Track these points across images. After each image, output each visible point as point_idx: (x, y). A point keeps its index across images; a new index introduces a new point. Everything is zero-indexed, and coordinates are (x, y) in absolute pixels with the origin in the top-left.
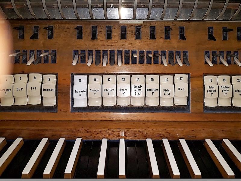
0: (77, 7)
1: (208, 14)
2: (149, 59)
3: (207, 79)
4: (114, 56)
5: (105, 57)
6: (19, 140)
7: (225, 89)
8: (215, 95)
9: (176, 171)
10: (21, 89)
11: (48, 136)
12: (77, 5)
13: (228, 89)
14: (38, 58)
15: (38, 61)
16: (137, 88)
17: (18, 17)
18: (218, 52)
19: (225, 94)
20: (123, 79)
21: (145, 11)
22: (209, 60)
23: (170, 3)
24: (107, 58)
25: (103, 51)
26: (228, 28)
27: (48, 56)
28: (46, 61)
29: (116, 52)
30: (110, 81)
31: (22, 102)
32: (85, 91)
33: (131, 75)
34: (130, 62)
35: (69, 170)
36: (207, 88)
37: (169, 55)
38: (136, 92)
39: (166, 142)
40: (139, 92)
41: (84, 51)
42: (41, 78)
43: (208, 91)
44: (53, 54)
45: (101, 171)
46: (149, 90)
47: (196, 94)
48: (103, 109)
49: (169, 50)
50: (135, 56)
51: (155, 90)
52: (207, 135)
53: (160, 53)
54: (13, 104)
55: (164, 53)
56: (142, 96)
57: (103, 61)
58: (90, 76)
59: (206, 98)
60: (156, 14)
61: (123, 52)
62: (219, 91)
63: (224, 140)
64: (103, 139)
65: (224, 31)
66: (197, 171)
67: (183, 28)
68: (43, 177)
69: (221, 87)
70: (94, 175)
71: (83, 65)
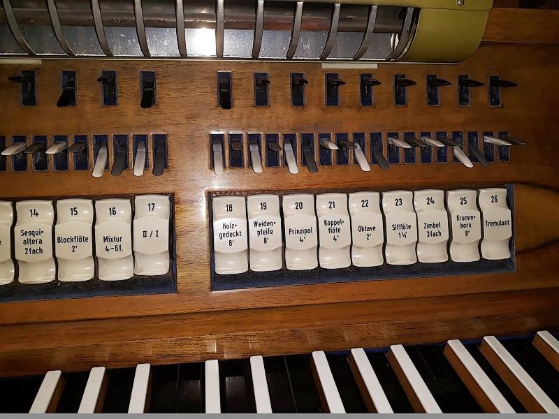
0: (105, 24)
2: (324, 150)
4: (125, 146)
7: (264, 228)
8: (240, 243)
12: (105, 18)
13: (271, 227)
16: (29, 237)
17: (22, 51)
19: (265, 240)
20: (152, 206)
22: (461, 154)
24: (147, 153)
25: (155, 135)
26: (438, 78)
27: (65, 151)
29: (245, 140)
30: (367, 206)
31: (117, 271)
32: (87, 239)
37: (231, 142)
38: (28, 246)
39: (360, 358)
40: (35, 247)
41: (85, 137)
42: (12, 215)
43: (222, 236)
46: (65, 241)
49: (486, 131)
51: (79, 239)
52: (257, 346)
53: (351, 138)
54: (51, 278)
60: (274, 47)
63: (449, 342)
64: (138, 366)
65: (397, 82)
69: (256, 224)
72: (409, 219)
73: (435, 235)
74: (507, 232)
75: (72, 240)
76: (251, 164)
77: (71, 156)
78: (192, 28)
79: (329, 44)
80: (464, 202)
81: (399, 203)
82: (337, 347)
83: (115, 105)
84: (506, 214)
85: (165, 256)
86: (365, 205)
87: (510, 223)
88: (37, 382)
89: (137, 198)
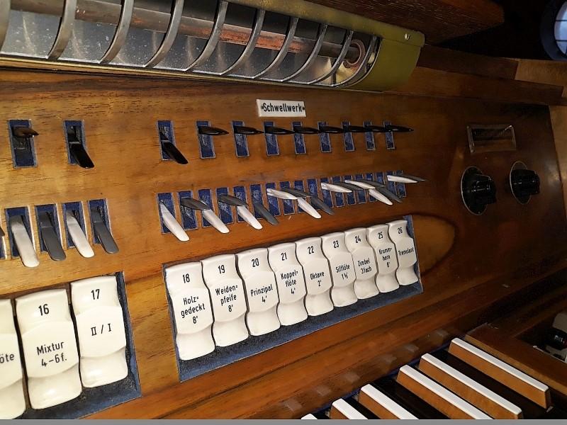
7: (227, 295)
8: (204, 318)
13: (233, 292)
26: (274, 125)
32: (12, 357)
36: (178, 307)
37: (40, 219)
38: (362, 267)
43: (184, 313)
47: (149, 332)
59: (184, 335)
65: (200, 132)
73: (367, 271)
74: (412, 258)
75: (200, 308)
78: (559, 105)
80: (381, 236)
83: (33, 165)
84: (409, 243)
85: (120, 354)
86: (311, 251)
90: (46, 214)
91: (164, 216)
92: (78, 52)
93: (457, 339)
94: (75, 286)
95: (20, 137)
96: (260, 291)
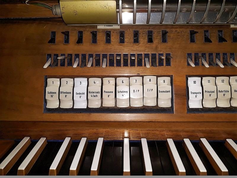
1: (206, 16)
2: (161, 60)
3: (191, 80)
5: (105, 60)
6: (41, 142)
8: (214, 96)
9: (202, 169)
10: (151, 90)
11: (86, 136)
14: (55, 61)
15: (56, 63)
18: (200, 55)
21: (145, 15)
23: (168, 8)
27: (64, 59)
28: (63, 65)
29: (101, 55)
32: (206, 91)
33: (129, 77)
34: (122, 65)
35: (95, 167)
37: (152, 58)
39: (187, 142)
44: (69, 57)
45: (127, 168)
48: (103, 110)
50: (133, 58)
51: (226, 91)
53: (200, 55)
55: (203, 55)
56: (99, 98)
57: (102, 64)
58: (90, 79)
59: (161, 99)
60: (155, 19)
61: (150, 55)
62: (205, 92)
63: (227, 140)
66: (223, 168)
67: (67, 34)
68: (146, 175)
70: (121, 172)
71: (70, 67)
72: (228, 88)
76: (145, 65)
77: (66, 60)
79: (177, 17)
81: (223, 81)
82: (178, 139)
87: (171, 91)
88: (60, 144)
89: (145, 77)
90: (211, 55)
91: (189, 61)
92: (181, 18)
93: (172, 139)
94: (145, 77)
95: (233, 33)
96: (80, 94)
